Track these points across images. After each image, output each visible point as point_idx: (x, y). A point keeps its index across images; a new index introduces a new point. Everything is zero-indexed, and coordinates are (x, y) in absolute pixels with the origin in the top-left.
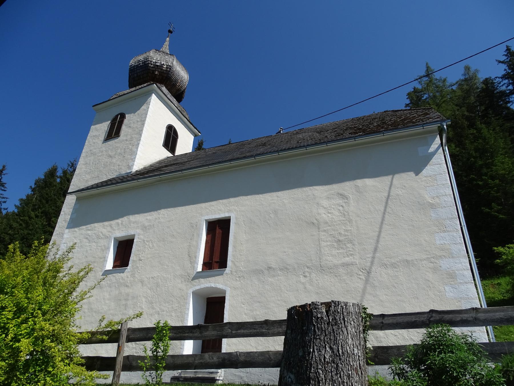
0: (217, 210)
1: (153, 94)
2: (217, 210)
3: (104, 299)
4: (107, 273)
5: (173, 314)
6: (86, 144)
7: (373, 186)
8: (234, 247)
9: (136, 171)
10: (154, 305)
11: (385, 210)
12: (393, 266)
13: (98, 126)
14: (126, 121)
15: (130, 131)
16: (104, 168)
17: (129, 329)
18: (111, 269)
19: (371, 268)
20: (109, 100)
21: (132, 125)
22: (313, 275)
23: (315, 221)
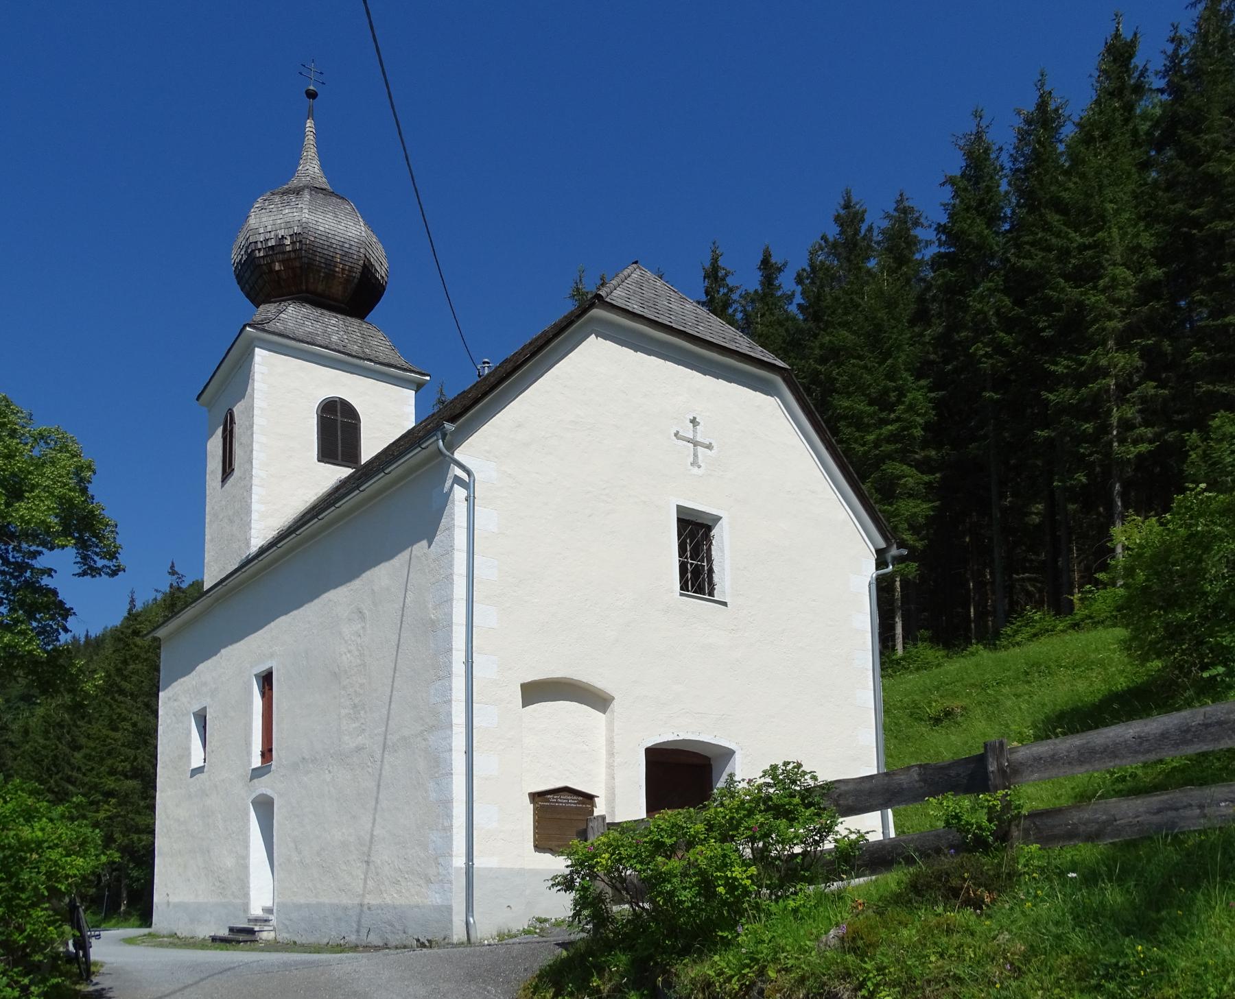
1: (257, 350)
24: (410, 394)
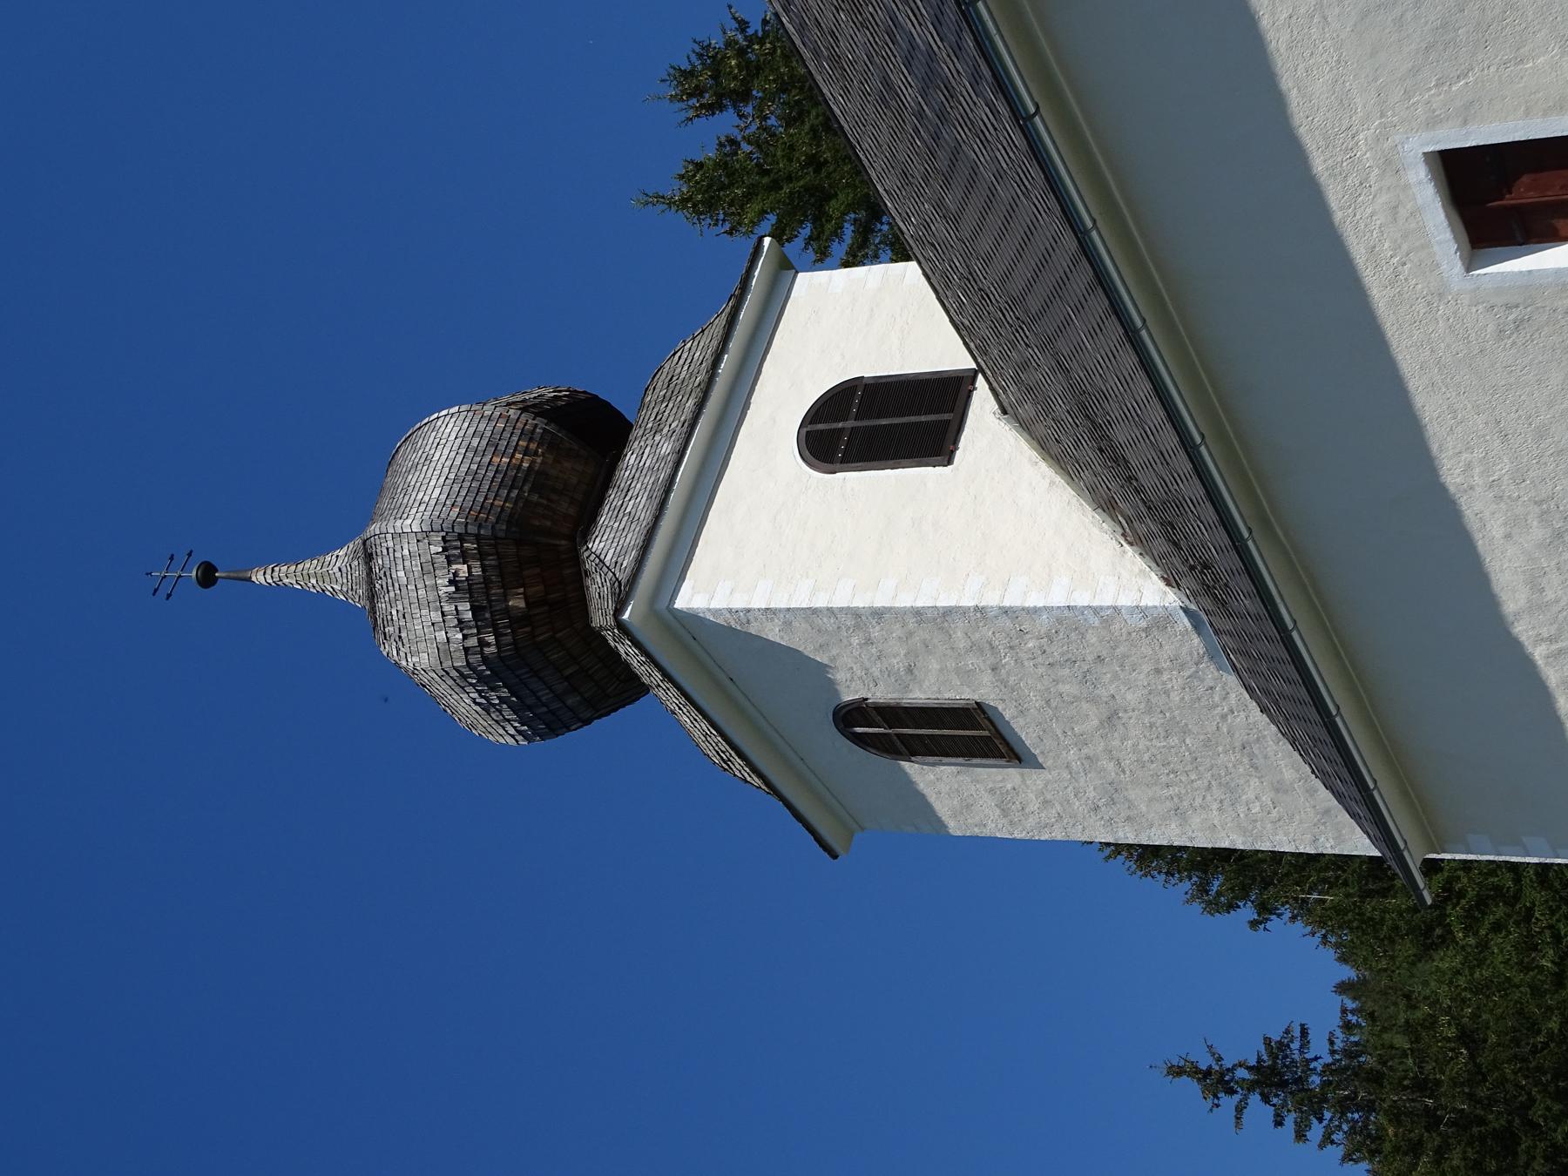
0: (1396, 230)
9: (1171, 581)
13: (943, 808)
14: (881, 694)
15: (935, 665)
16: (1185, 731)
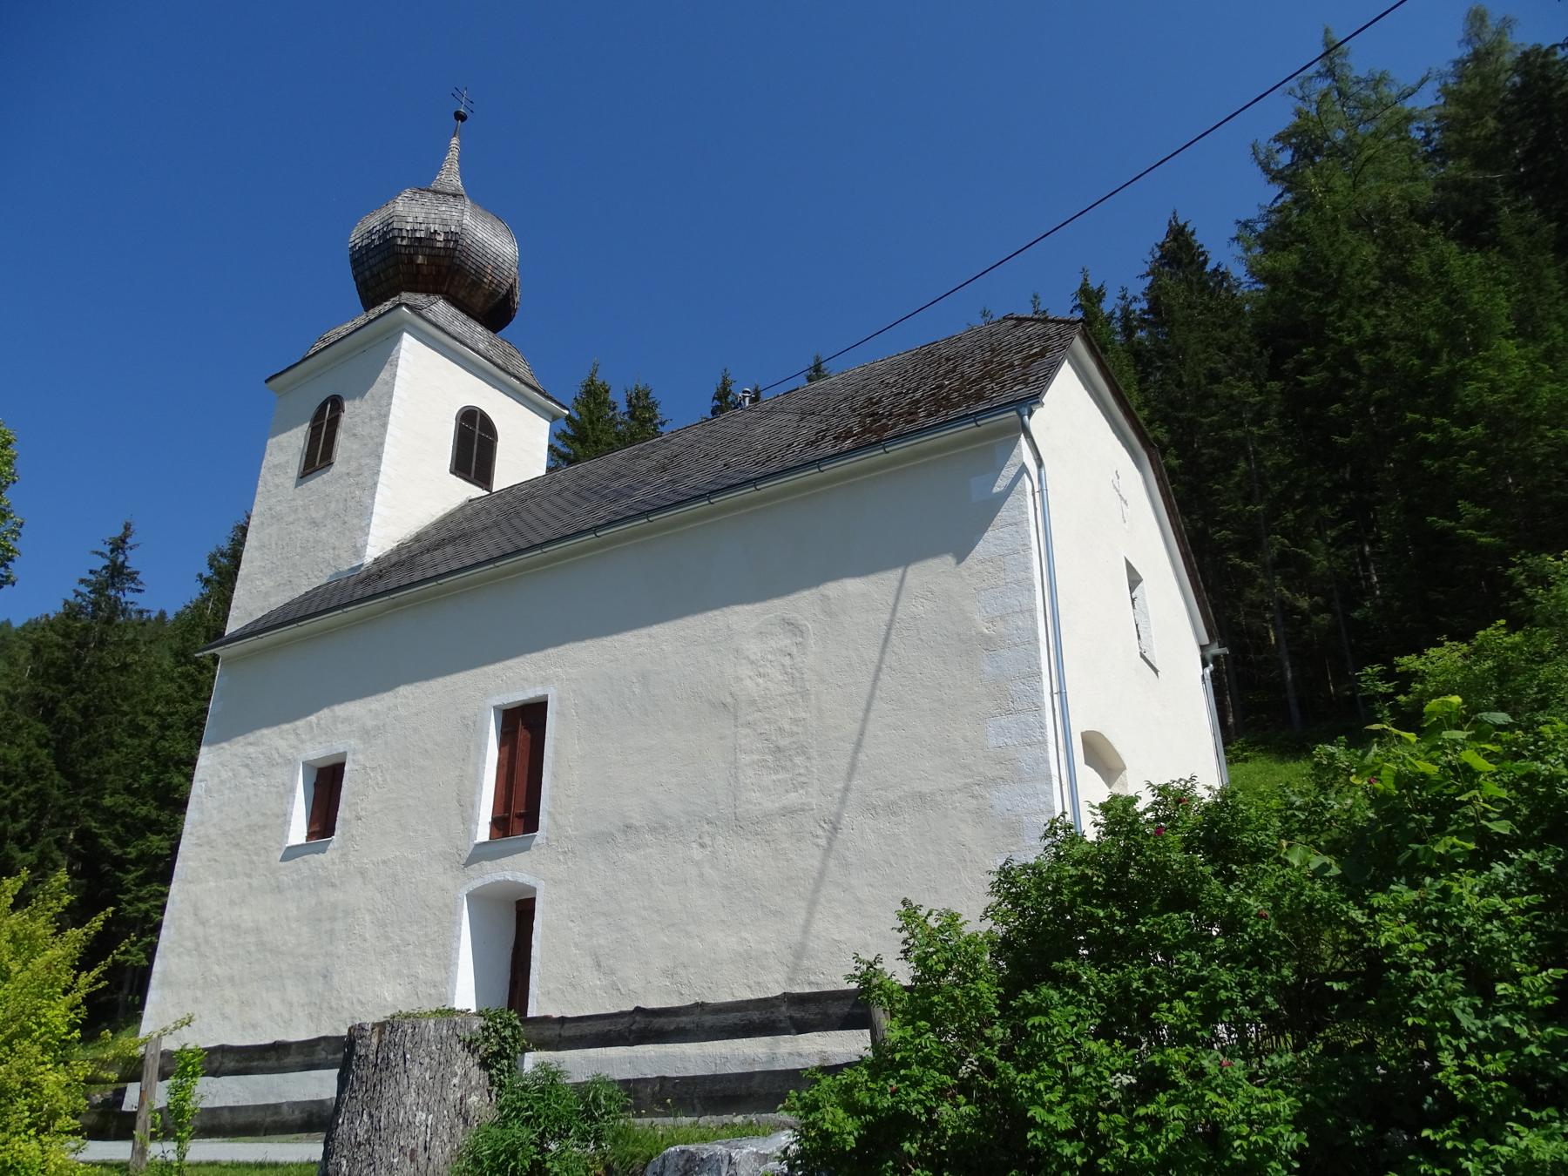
0: (516, 680)
1: (405, 335)
2: (516, 680)
3: (287, 918)
4: (292, 853)
5: (428, 951)
6: (259, 490)
7: (860, 594)
8: (555, 775)
10: (389, 929)
11: (881, 660)
12: (892, 809)
13: (282, 438)
14: (344, 420)
16: (302, 556)
17: (163, 1054)
18: (303, 841)
19: (839, 816)
20: (305, 359)
21: (358, 430)
22: (720, 840)
23: (729, 700)
24: (543, 426)
